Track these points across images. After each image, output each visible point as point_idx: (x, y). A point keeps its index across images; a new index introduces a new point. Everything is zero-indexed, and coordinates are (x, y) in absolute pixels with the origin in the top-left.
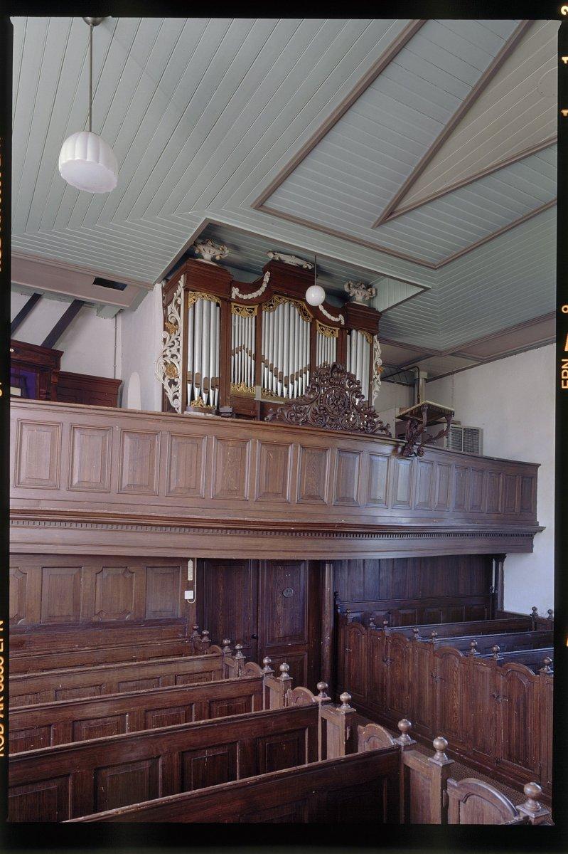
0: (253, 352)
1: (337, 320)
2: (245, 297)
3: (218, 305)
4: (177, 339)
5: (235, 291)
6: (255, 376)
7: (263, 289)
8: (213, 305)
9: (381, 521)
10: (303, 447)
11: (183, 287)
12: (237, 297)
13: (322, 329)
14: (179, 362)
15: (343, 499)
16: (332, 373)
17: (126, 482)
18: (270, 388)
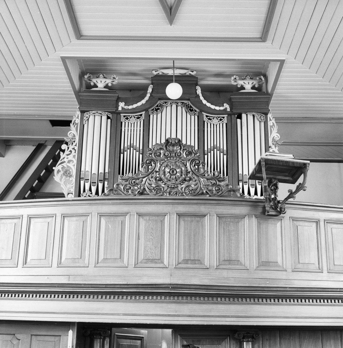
1: (222, 108)
2: (130, 107)
3: (108, 118)
4: (74, 149)
5: (122, 105)
7: (147, 98)
8: (104, 118)
10: (140, 215)
15: (229, 261)
16: (166, 148)
17: (141, 257)
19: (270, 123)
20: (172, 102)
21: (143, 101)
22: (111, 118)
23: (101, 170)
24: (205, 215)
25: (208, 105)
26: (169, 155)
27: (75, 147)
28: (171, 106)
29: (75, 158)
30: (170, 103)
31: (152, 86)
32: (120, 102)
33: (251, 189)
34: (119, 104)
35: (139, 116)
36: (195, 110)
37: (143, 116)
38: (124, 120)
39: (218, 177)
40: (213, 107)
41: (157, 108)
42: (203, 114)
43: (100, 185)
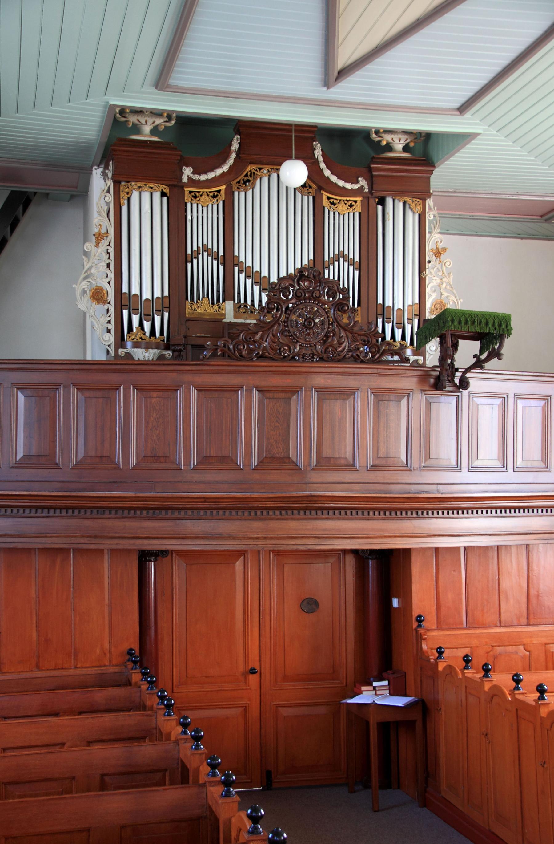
0: (221, 253)
1: (356, 186)
2: (203, 177)
3: (163, 194)
5: (187, 171)
6: (224, 291)
7: (231, 161)
8: (157, 196)
9: (396, 491)
11: (112, 179)
12: (189, 178)
13: (331, 203)
14: (109, 283)
18: (249, 302)
19: (430, 216)
20: (271, 169)
21: (225, 168)
22: (168, 195)
23: (158, 294)
24: (355, 391)
25: (334, 179)
26: (303, 295)
27: (108, 247)
28: (269, 176)
29: (110, 269)
30: (268, 170)
31: (239, 137)
32: (184, 167)
33: (396, 330)
34: (183, 171)
35: (216, 193)
36: (309, 185)
37: (223, 192)
38: (190, 200)
39: (374, 332)
40: (341, 183)
41: (246, 178)
42: (323, 194)
43: (157, 319)
